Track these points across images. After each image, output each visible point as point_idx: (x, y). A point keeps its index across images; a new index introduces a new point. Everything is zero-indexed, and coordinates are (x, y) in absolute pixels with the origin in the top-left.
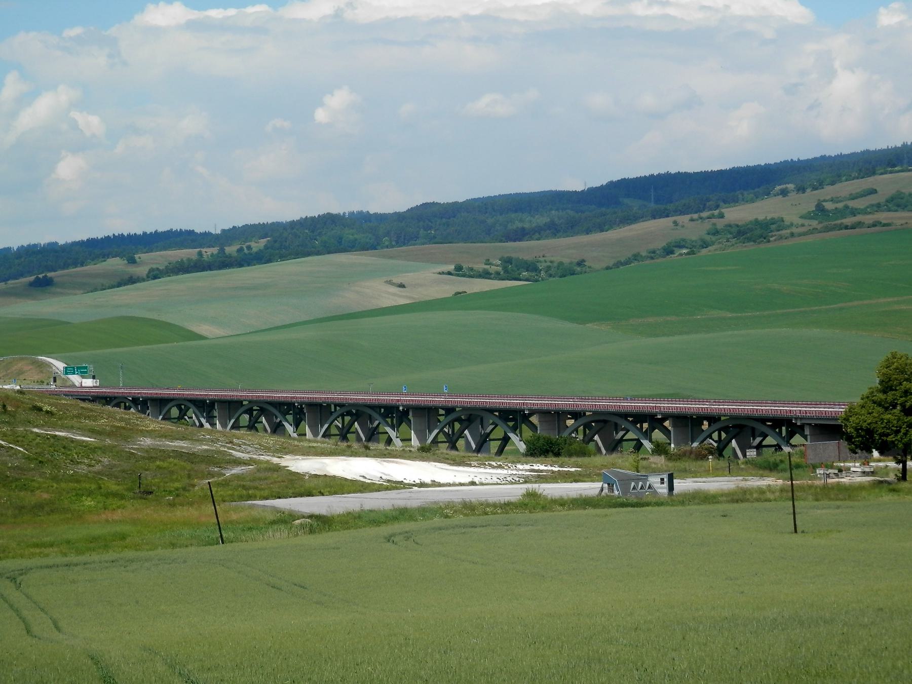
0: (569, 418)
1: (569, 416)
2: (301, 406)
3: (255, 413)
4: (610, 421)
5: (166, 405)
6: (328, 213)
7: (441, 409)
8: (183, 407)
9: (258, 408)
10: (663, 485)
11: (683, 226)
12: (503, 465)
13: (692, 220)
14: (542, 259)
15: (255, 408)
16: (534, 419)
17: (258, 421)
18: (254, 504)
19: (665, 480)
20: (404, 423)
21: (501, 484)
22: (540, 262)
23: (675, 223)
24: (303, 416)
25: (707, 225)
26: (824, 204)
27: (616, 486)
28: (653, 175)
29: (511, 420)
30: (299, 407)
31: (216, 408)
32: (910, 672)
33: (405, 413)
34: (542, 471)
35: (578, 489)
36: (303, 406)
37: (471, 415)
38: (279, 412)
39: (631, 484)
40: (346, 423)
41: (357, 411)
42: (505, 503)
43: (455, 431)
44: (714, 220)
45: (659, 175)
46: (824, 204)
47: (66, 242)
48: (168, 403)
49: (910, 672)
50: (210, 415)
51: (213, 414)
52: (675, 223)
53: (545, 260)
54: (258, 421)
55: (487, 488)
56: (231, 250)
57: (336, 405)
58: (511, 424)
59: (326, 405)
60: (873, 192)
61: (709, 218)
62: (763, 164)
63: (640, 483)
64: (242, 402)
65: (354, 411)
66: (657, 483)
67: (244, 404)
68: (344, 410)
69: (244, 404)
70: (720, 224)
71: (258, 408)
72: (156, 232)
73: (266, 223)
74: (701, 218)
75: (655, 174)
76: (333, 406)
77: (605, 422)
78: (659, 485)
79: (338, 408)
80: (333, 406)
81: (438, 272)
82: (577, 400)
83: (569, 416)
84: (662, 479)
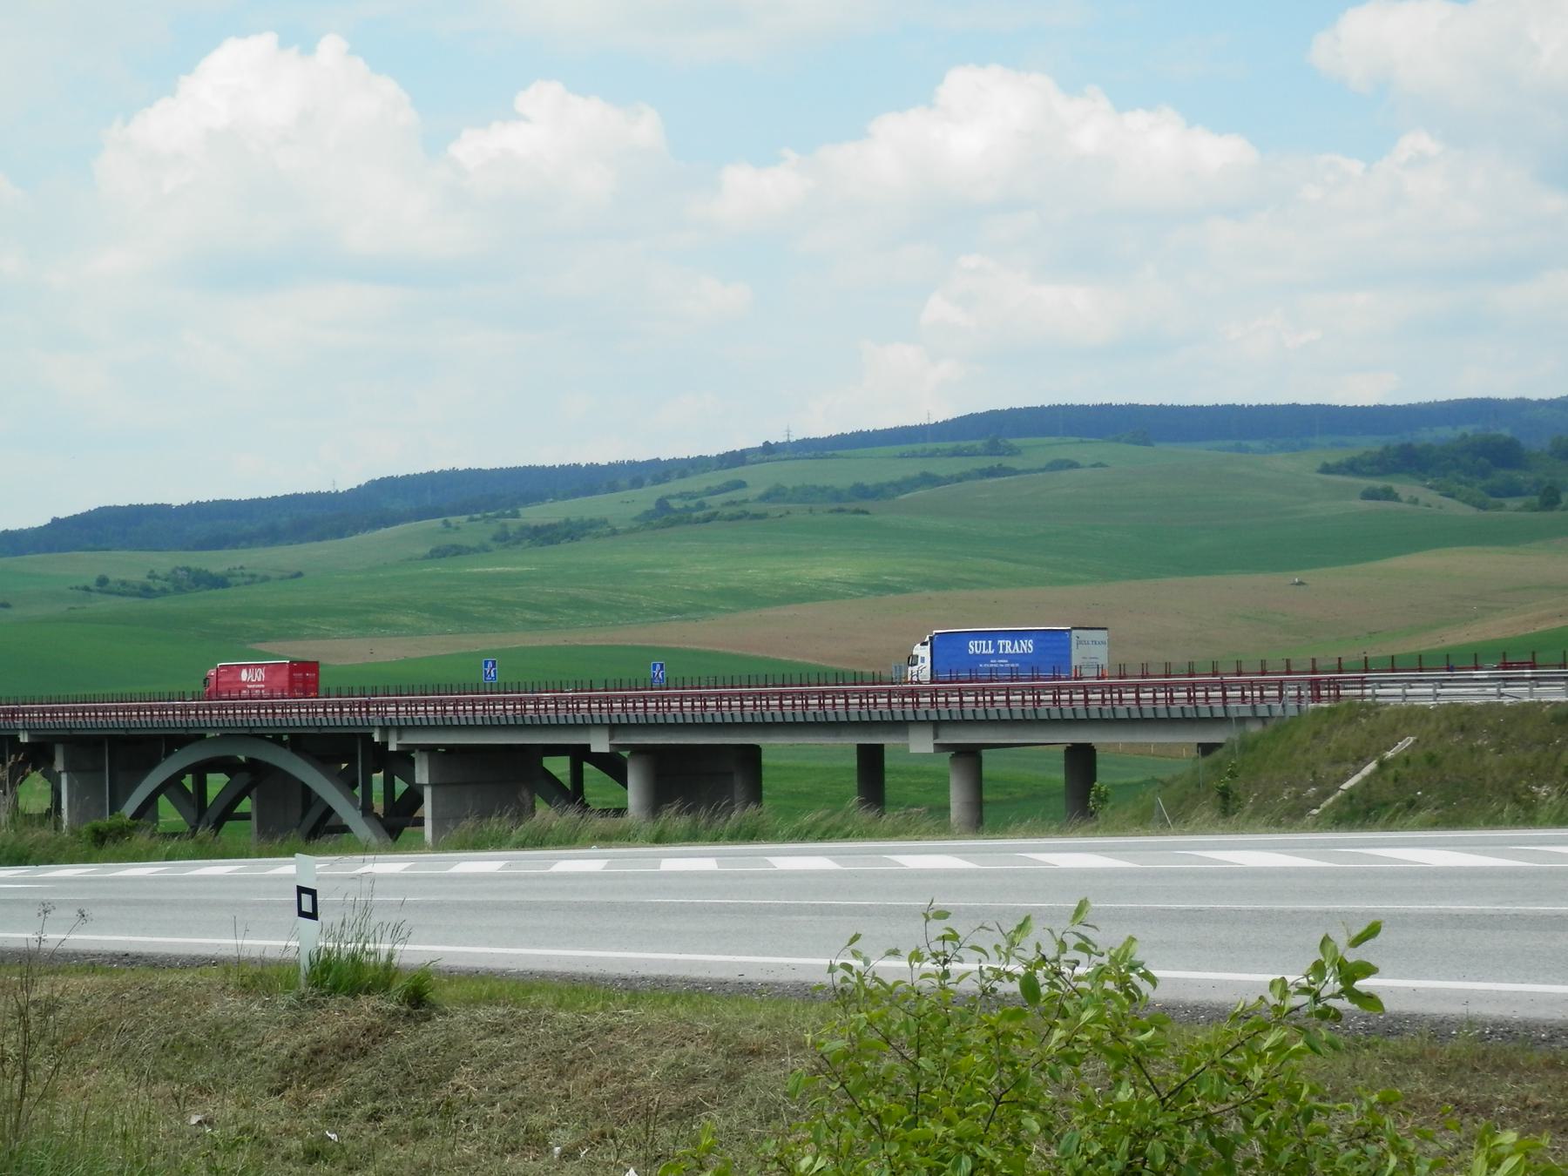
4: (627, 788)
5: (151, 764)
7: (1249, 717)
11: (457, 528)
13: (471, 520)
17: (237, 810)
23: (447, 524)
25: (494, 528)
26: (668, 500)
28: (432, 472)
42: (421, 996)
44: (502, 520)
45: (441, 472)
46: (668, 500)
48: (169, 753)
52: (447, 524)
54: (237, 810)
55: (1234, 974)
60: (741, 485)
61: (497, 516)
70: (513, 525)
74: (485, 517)
75: (436, 471)
81: (898, 454)
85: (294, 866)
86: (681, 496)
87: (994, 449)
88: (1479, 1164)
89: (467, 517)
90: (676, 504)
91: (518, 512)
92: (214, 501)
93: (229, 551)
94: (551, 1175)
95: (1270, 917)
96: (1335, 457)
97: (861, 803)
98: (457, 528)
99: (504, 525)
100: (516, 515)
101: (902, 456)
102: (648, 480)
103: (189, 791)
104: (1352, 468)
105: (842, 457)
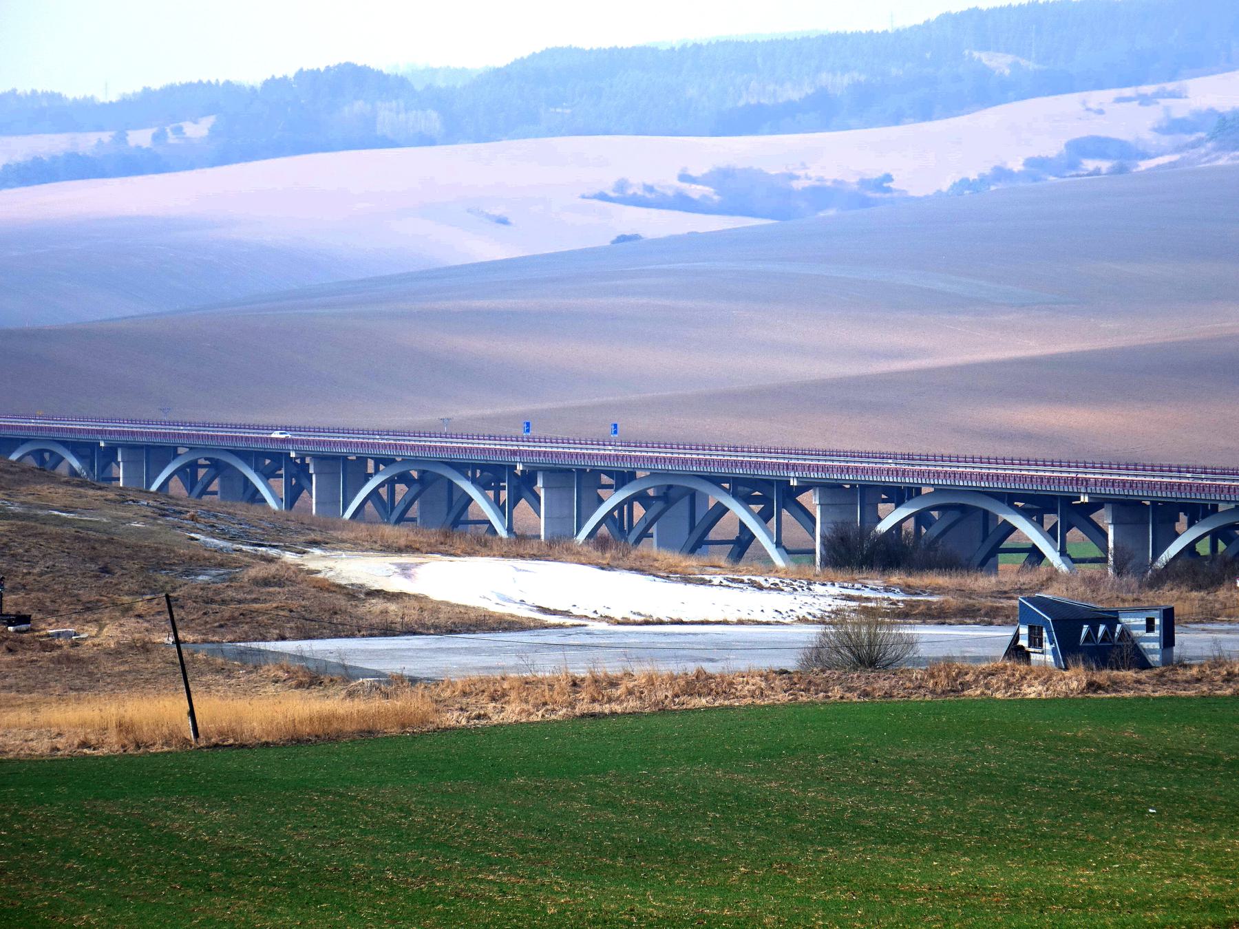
0: (884, 501)
1: (884, 496)
2: (303, 460)
3: (202, 472)
6: (347, 64)
8: (47, 455)
9: (207, 462)
10: (1151, 635)
12: (781, 585)
13: (1120, 100)
14: (801, 173)
15: (202, 462)
16: (811, 500)
18: (251, 649)
19: (1157, 622)
20: (523, 501)
21: (784, 624)
22: (798, 178)
24: (305, 482)
27: (1049, 632)
29: (756, 501)
30: (298, 461)
31: (120, 459)
32: (686, 924)
33: (528, 479)
34: (868, 599)
35: (957, 640)
36: (308, 460)
37: (670, 487)
38: (256, 471)
39: (1082, 628)
40: (398, 498)
41: (423, 473)
43: (636, 521)
47: (273, 76)
49: (686, 924)
50: (104, 476)
51: (111, 472)
53: (806, 174)
56: (141, 138)
57: (378, 461)
58: (757, 508)
59: (354, 458)
62: (359, 65)
63: (1102, 628)
64: (175, 448)
65: (415, 474)
66: (1138, 627)
67: (179, 452)
68: (394, 471)
69: (179, 452)
70: (1180, 109)
71: (207, 462)
72: (547, 48)
73: (213, 82)
76: (371, 464)
77: (963, 508)
78: (1142, 633)
79: (382, 467)
80: (371, 464)
82: (902, 461)
83: (884, 496)
84: (1150, 622)
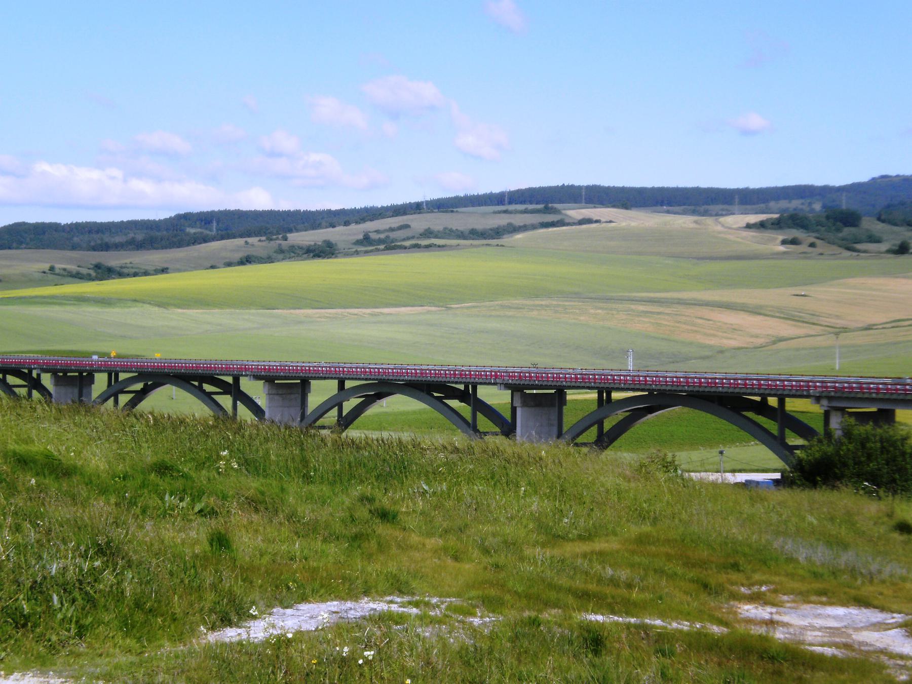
13: (260, 241)
23: (246, 243)
25: (274, 244)
52: (246, 243)
60: (407, 226)
85: (780, 474)
86: (377, 232)
87: (547, 210)
88: (908, 585)
89: (258, 238)
90: (374, 236)
91: (286, 236)
92: (86, 222)
93: (113, 252)
94: (670, 683)
95: (94, 456)
96: (754, 219)
97: (566, 405)
98: (253, 245)
99: (280, 245)
100: (285, 239)
101: (495, 213)
102: (737, 200)
103: (630, 415)
104: (777, 225)
105: (461, 212)
